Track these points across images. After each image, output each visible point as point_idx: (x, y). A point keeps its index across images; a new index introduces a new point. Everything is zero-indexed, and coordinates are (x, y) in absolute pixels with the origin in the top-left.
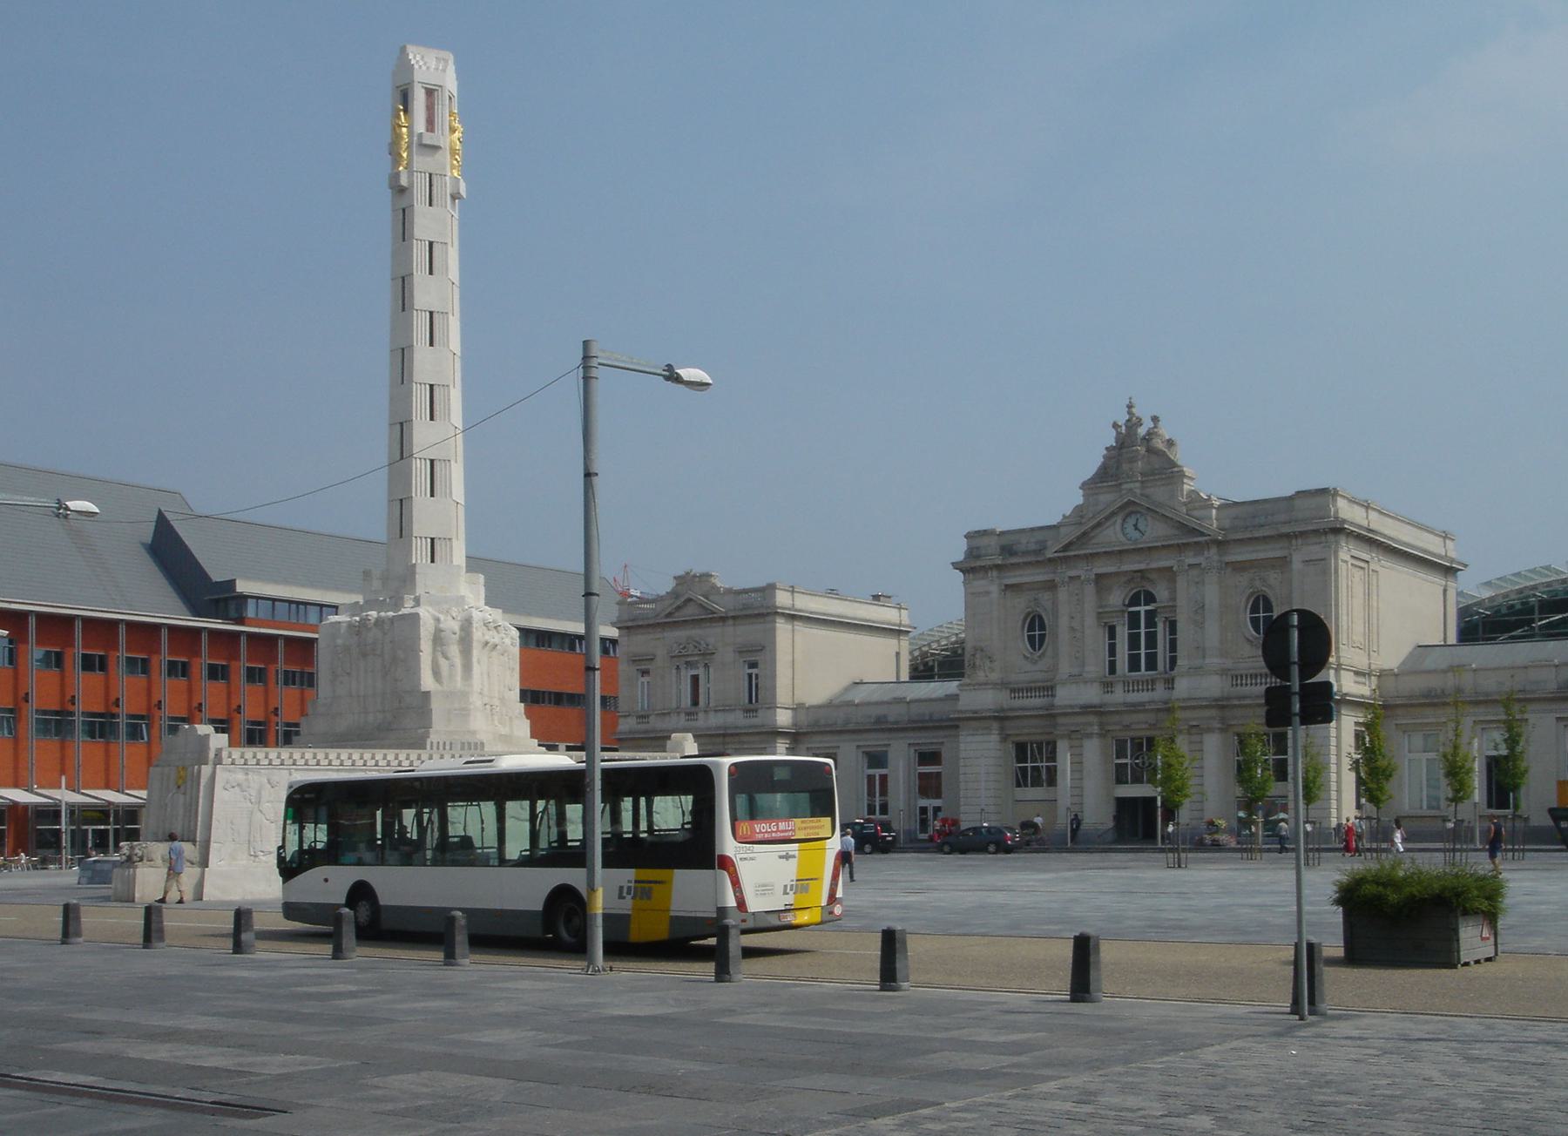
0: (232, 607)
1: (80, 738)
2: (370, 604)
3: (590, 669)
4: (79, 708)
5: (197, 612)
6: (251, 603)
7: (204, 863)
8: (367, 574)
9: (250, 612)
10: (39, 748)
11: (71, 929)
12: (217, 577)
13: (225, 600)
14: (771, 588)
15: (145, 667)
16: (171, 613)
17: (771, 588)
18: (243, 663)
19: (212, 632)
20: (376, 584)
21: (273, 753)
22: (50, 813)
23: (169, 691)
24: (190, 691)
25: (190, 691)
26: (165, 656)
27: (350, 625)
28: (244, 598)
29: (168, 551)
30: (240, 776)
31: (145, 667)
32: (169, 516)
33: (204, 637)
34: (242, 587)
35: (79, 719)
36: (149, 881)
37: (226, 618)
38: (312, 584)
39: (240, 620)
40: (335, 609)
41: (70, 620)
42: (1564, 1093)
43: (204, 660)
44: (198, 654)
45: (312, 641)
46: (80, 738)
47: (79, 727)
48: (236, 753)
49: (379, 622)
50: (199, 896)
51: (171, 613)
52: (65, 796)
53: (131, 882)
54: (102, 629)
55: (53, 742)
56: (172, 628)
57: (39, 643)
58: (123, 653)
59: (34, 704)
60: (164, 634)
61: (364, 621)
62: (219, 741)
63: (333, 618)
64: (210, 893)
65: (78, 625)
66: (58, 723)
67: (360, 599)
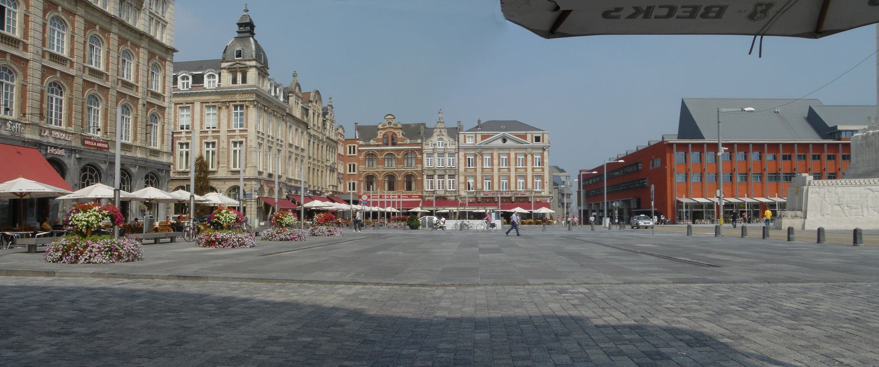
0: (836, 135)
1: (782, 182)
2: (870, 128)
3: (127, 180)
4: (782, 172)
5: (824, 138)
6: (843, 133)
7: (805, 218)
8: (869, 118)
9: (843, 136)
10: (769, 185)
11: (821, 238)
12: (830, 125)
13: (834, 133)
14: (418, 132)
15: (819, 157)
16: (811, 138)
17: (418, 132)
18: (811, 154)
19: (828, 144)
20: (873, 121)
21: (825, 182)
22: (741, 205)
23: (797, 163)
24: (821, 164)
25: (821, 164)
26: (811, 154)
27: (862, 136)
28: (841, 131)
29: (813, 119)
30: (817, 189)
31: (819, 157)
32: (814, 108)
33: (826, 146)
34: (840, 128)
35: (782, 175)
36: (786, 223)
37: (834, 139)
38: (853, 124)
39: (839, 139)
40: (857, 131)
41: (778, 145)
42: (3, 342)
43: (825, 154)
44: (838, 152)
45: (849, 144)
46: (782, 182)
47: (782, 178)
48: (816, 182)
49: (873, 134)
50: (803, 228)
51: (811, 138)
52: (748, 200)
53: (781, 224)
54: (789, 147)
55: (774, 183)
56: (813, 144)
57: (768, 152)
58: (796, 154)
59: (752, 171)
60: (811, 146)
61: (867, 135)
62: (809, 178)
63: (855, 135)
64: (807, 227)
65: (811, 146)
66: (775, 177)
67: (867, 127)
